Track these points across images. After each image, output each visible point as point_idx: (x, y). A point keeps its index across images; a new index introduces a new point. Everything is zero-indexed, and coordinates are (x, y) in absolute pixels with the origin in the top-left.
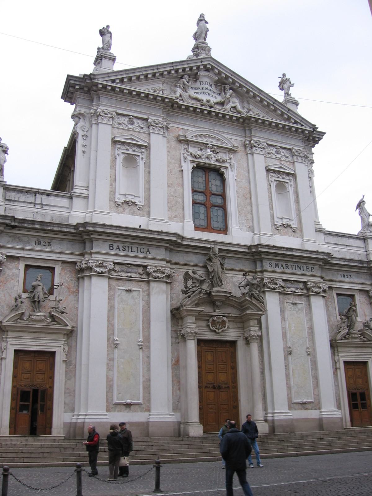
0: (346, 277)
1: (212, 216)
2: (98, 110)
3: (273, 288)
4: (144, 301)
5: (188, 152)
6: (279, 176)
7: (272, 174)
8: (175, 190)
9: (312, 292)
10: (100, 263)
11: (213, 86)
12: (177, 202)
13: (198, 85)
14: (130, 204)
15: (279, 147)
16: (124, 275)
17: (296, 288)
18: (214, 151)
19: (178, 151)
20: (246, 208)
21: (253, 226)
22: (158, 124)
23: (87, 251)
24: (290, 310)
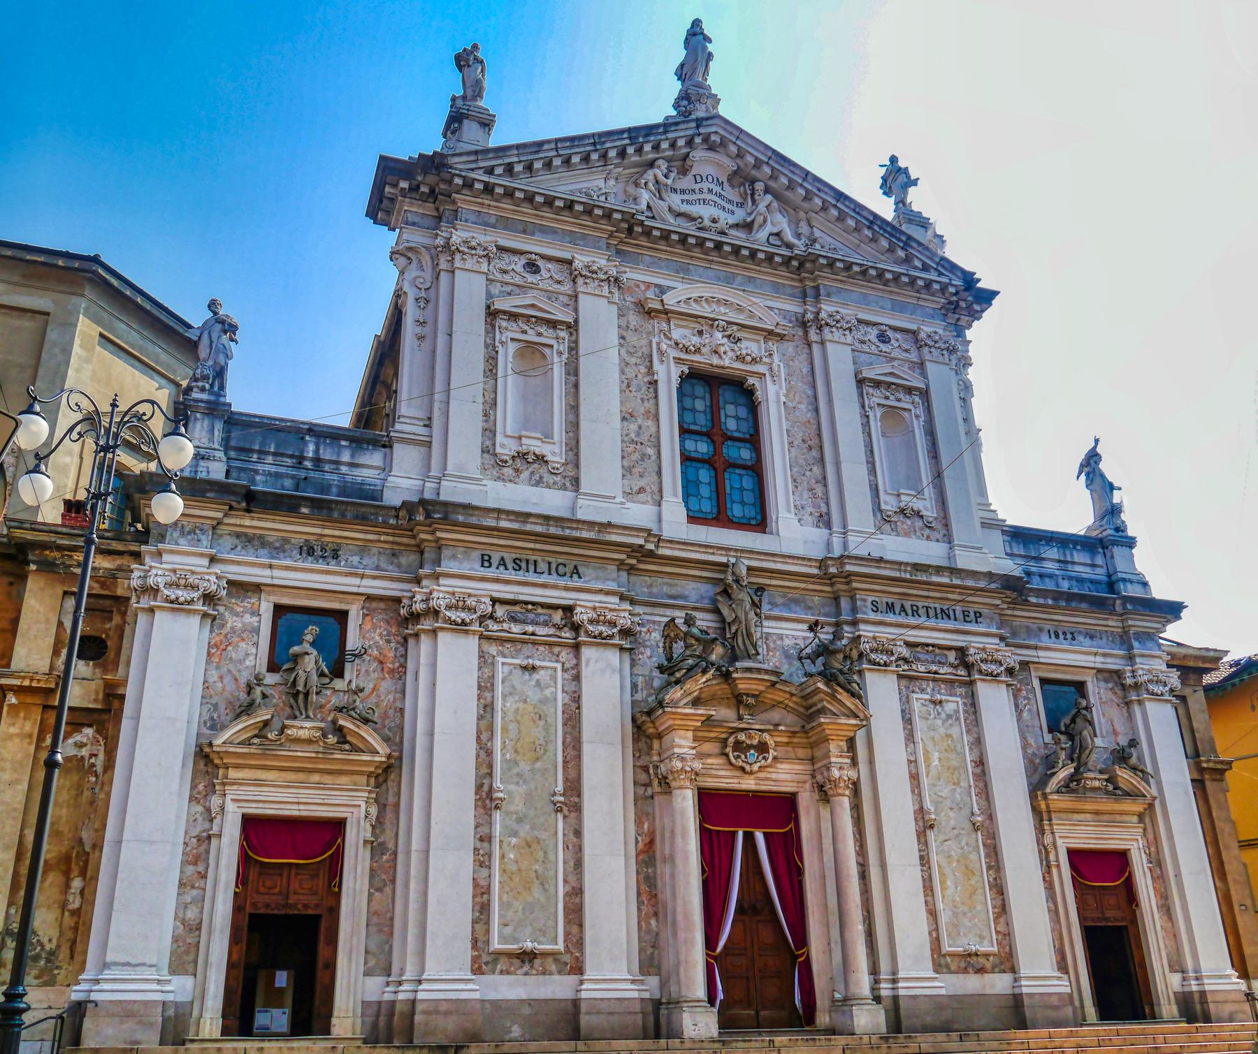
0: (1062, 636)
5: (670, 339)
8: (640, 427)
11: (726, 184)
12: (644, 456)
13: (686, 182)
16: (516, 628)
17: (940, 663)
20: (811, 470)
21: (828, 514)
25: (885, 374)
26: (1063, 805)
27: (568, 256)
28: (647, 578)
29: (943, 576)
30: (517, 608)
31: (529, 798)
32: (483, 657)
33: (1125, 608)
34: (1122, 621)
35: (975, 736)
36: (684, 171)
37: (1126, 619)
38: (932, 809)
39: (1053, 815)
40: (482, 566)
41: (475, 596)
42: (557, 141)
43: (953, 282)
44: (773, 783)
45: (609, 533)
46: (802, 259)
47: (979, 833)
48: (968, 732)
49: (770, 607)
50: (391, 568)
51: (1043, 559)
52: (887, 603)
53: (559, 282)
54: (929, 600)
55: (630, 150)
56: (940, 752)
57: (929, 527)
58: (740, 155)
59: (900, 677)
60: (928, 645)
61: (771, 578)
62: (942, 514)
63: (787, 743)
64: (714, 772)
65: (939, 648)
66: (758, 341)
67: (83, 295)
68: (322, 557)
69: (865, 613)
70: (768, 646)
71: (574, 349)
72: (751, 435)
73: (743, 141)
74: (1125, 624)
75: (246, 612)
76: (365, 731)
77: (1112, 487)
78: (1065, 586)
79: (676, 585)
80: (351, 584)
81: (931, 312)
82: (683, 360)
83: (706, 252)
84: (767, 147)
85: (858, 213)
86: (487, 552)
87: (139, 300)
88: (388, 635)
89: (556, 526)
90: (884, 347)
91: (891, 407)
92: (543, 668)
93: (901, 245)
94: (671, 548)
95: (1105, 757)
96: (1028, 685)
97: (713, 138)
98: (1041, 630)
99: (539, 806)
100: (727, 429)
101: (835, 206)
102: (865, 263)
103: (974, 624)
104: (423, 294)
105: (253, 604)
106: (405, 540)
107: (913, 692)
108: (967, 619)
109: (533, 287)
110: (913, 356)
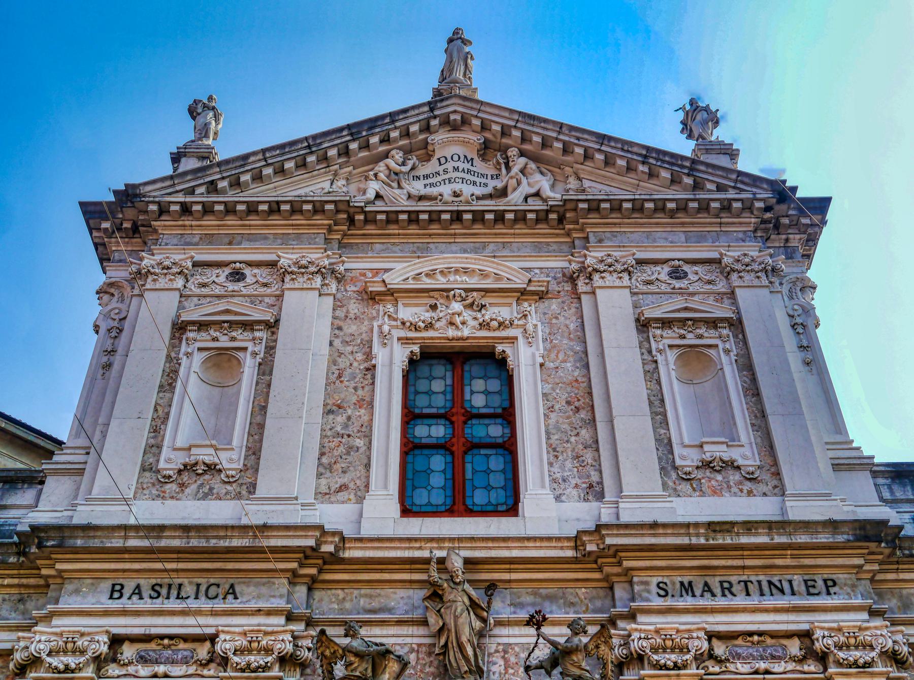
1: (469, 475)
2: (589, 261)
3: (61, 667)
5: (395, 320)
8: (349, 418)
11: (477, 161)
12: (350, 449)
13: (431, 167)
15: (681, 263)
17: (773, 657)
18: (473, 303)
19: (366, 323)
20: (578, 434)
21: (601, 483)
22: (307, 267)
23: (620, 609)
25: (678, 311)
28: (339, 592)
29: (757, 534)
30: (153, 646)
36: (428, 157)
40: (111, 598)
41: (89, 634)
42: (264, 151)
43: (758, 196)
45: (268, 537)
49: (512, 609)
50: (13, 615)
52: (682, 583)
54: (747, 572)
55: (354, 146)
57: (750, 480)
58: (484, 127)
60: (751, 634)
61: (510, 571)
62: (769, 461)
65: (772, 637)
66: (510, 305)
69: (648, 600)
70: (506, 661)
71: (270, 349)
72: (504, 409)
84: (512, 111)
85: (628, 151)
86: (121, 581)
89: (199, 537)
93: (686, 171)
101: (599, 150)
103: (824, 595)
104: (116, 324)
106: (32, 581)
108: (812, 590)
109: (234, 294)
110: (721, 286)
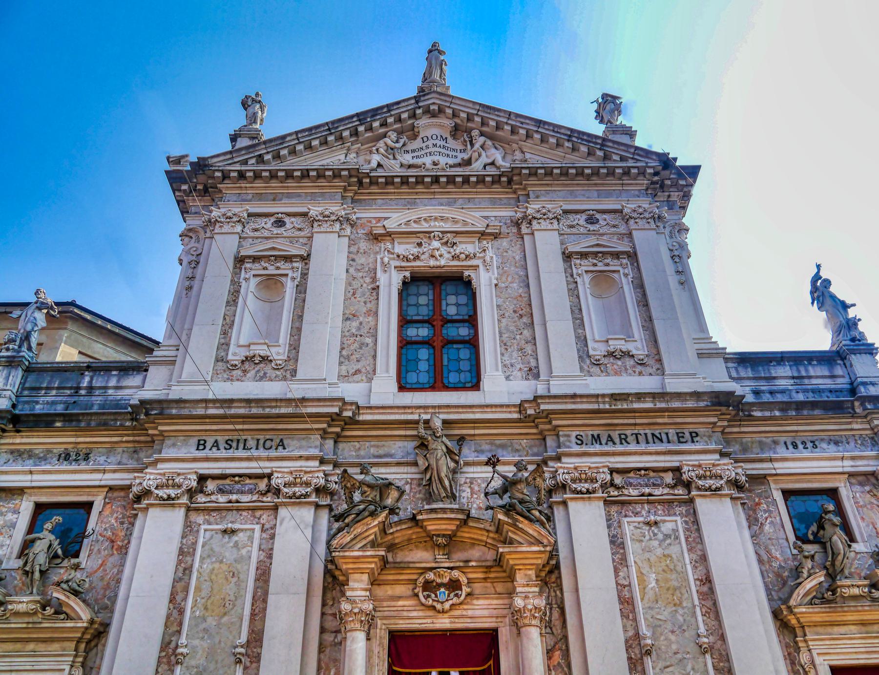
0: (801, 446)
1: (445, 362)
4: (263, 550)
5: (393, 254)
6: (595, 261)
7: (578, 261)
8: (361, 323)
9: (699, 489)
10: (295, 478)
11: (450, 139)
12: (362, 345)
13: (417, 144)
14: (257, 362)
16: (222, 499)
17: (654, 485)
18: (448, 241)
19: (372, 256)
21: (537, 367)
24: (642, 541)
25: (592, 246)
26: (817, 618)
27: (305, 210)
28: (356, 443)
29: (644, 402)
30: (228, 481)
31: (211, 654)
32: (190, 526)
33: (865, 409)
34: (869, 422)
35: (700, 553)
36: (414, 137)
37: (872, 419)
38: (649, 634)
39: (807, 630)
40: (198, 449)
41: (183, 474)
42: (297, 133)
43: (649, 165)
44: (469, 620)
46: (510, 174)
47: (708, 656)
48: (690, 550)
51: (775, 378)
52: (593, 436)
53: (300, 229)
54: (637, 427)
55: (361, 129)
56: (657, 573)
58: (455, 115)
59: (607, 503)
60: (639, 469)
61: (474, 428)
63: (485, 579)
64: (405, 614)
65: (654, 471)
66: (474, 243)
67: (66, 329)
68: (75, 460)
69: (569, 447)
71: (305, 275)
73: (455, 104)
74: (872, 425)
75: (9, 512)
76: (74, 601)
77: (845, 306)
78: (801, 397)
79: (384, 446)
80: (95, 479)
81: (637, 193)
82: (404, 267)
83: (428, 186)
84: (474, 103)
85: (558, 132)
87: (109, 327)
88: (123, 518)
89: (258, 407)
90: (592, 227)
91: (600, 271)
92: (242, 530)
93: (599, 146)
94: (371, 414)
95: (869, 563)
96: (769, 497)
97: (432, 107)
98: (776, 443)
99: (220, 658)
100: (448, 315)
102: (564, 165)
103: (690, 443)
105: (17, 504)
106: (142, 438)
107: (626, 516)
110: (622, 229)
